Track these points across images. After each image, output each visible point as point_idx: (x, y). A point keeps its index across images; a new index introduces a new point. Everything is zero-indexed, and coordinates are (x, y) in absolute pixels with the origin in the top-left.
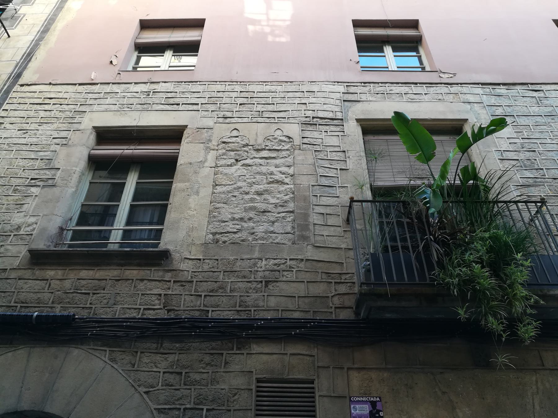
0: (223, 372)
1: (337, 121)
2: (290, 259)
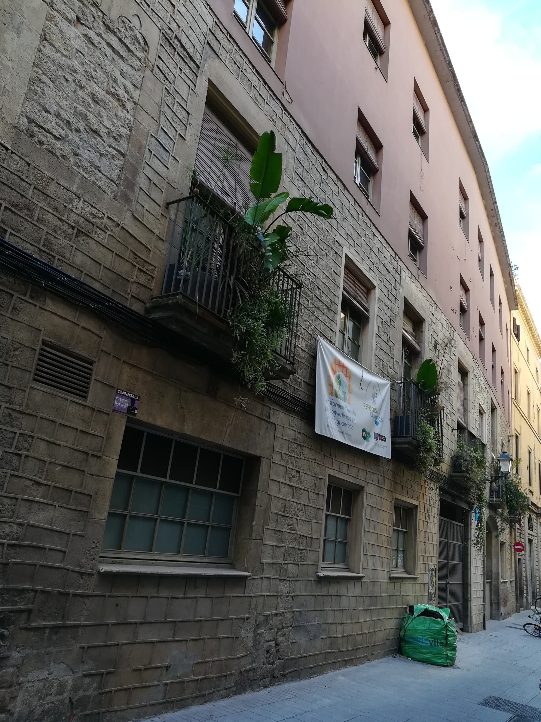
0: (9, 318)
1: (193, 64)
2: (108, 217)
